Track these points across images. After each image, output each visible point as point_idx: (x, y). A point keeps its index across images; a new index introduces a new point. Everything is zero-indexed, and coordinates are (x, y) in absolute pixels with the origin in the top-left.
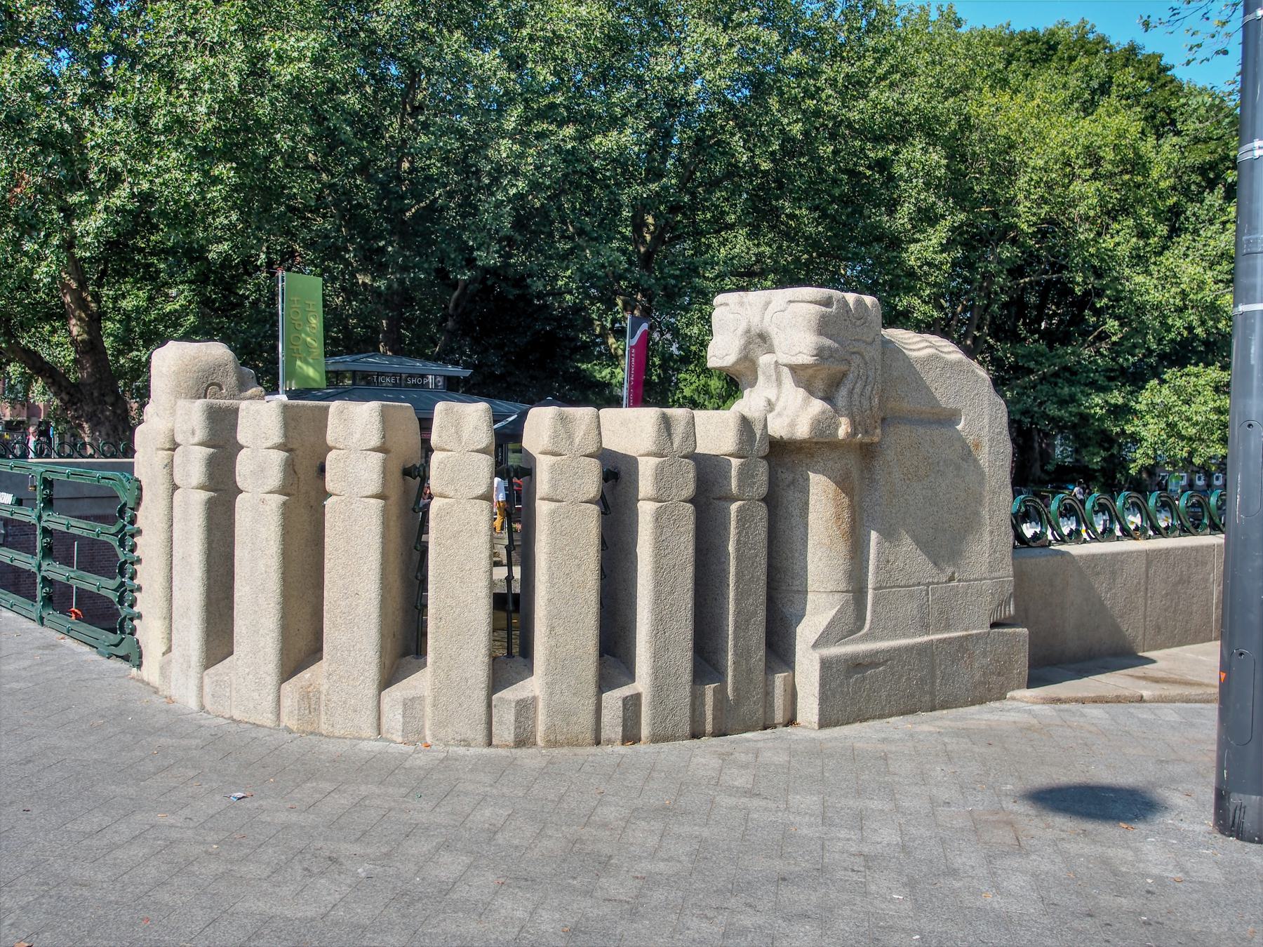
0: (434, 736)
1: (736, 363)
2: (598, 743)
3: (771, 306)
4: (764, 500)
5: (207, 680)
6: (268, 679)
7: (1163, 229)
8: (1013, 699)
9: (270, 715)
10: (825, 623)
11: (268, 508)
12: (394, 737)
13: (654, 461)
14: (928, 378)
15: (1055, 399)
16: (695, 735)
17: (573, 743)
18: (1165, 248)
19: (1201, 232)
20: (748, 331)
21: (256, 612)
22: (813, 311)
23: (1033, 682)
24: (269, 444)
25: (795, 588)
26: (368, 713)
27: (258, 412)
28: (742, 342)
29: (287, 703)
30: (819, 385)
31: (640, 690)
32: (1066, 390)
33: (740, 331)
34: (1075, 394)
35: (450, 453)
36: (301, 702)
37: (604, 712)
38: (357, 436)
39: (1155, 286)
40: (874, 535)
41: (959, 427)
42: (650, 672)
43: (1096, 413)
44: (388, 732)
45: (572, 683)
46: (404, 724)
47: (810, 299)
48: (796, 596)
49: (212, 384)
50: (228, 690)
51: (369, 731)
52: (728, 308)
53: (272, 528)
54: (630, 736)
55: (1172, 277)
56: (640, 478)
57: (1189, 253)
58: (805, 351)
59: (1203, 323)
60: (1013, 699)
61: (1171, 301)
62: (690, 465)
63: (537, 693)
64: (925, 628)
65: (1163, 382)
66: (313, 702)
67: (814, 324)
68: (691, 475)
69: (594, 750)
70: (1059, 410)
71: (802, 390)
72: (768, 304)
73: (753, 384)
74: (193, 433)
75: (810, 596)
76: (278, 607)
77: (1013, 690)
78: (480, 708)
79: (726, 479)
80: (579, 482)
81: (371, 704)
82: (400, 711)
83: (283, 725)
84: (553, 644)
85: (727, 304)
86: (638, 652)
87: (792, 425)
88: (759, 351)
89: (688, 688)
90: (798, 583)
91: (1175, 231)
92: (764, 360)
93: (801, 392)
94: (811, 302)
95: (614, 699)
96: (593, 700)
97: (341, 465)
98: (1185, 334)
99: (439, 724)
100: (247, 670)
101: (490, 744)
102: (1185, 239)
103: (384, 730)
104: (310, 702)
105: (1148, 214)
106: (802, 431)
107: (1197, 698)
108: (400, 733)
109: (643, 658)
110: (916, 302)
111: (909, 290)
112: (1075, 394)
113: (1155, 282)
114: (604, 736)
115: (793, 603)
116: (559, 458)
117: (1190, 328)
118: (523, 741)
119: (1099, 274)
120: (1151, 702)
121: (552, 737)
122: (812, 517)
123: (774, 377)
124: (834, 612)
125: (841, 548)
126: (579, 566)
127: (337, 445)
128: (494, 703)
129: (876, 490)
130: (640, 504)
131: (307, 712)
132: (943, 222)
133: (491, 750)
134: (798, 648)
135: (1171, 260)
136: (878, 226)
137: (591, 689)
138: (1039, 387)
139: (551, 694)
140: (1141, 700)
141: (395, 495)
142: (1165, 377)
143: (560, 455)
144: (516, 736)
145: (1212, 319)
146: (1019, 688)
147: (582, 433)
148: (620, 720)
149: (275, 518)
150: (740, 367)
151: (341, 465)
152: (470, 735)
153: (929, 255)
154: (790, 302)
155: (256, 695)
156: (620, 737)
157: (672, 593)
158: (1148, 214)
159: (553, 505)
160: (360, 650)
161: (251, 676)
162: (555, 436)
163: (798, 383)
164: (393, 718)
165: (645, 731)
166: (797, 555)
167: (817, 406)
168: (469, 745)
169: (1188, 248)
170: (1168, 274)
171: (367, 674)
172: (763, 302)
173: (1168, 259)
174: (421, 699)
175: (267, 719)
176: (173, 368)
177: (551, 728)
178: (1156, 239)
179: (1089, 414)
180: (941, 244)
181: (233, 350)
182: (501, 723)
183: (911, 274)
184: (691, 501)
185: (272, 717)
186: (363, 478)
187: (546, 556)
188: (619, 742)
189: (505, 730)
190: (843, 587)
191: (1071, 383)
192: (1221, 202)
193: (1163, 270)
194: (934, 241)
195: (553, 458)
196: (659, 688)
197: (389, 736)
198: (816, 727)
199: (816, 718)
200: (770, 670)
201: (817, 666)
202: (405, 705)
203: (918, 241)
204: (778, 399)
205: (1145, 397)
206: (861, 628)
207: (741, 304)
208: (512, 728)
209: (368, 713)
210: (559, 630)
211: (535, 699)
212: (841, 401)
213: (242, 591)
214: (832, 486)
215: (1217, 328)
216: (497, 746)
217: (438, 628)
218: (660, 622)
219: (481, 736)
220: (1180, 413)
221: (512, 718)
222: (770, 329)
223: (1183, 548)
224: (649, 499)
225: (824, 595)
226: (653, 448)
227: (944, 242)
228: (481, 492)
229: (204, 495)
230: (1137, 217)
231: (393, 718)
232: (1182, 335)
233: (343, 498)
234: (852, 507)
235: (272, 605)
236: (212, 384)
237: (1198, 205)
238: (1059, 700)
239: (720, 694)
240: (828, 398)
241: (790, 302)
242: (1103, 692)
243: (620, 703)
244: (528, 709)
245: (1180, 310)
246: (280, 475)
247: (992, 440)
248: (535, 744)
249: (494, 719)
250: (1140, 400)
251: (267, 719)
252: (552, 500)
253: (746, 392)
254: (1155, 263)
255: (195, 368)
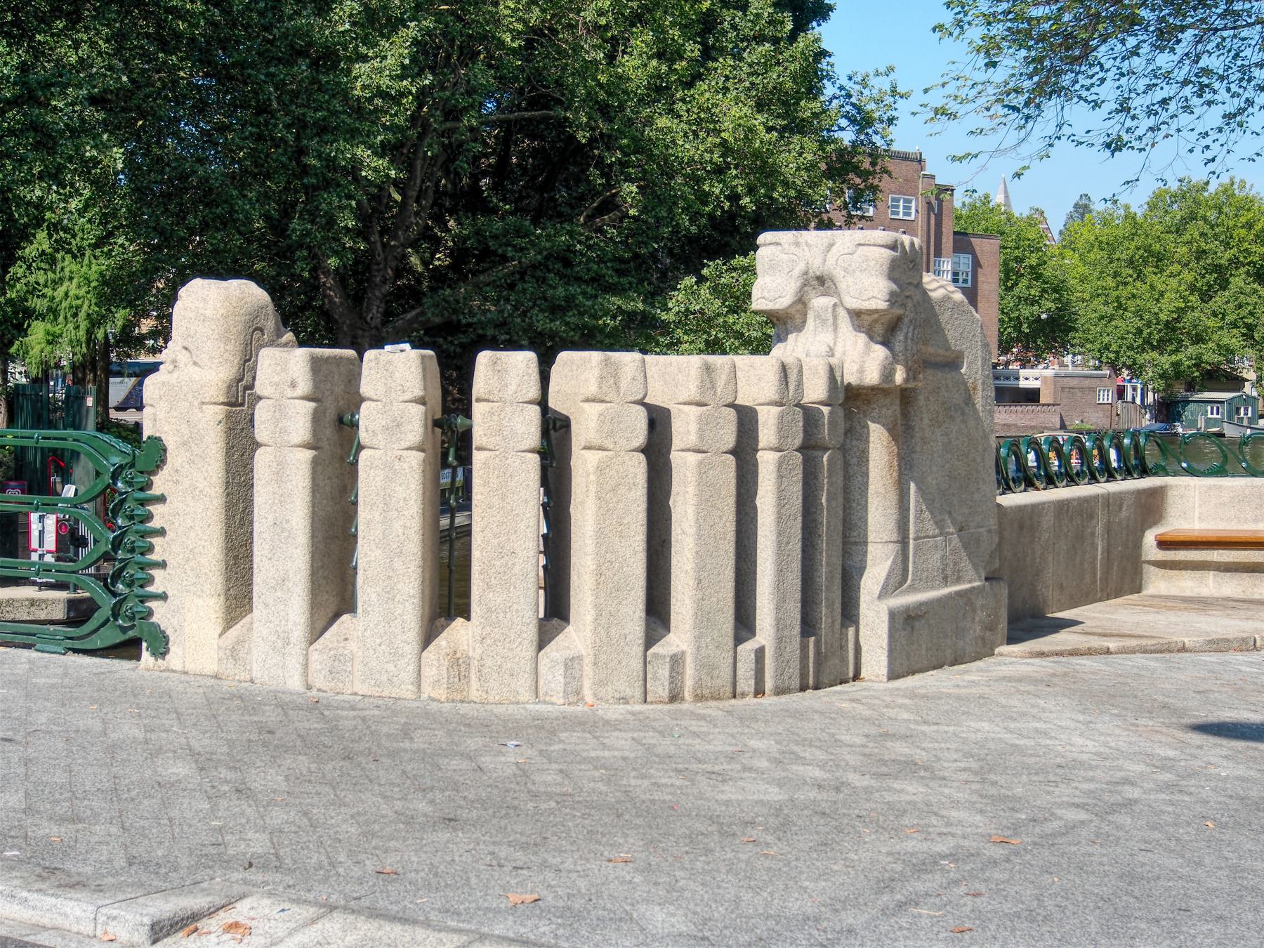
0: (595, 695)
1: (791, 306)
2: (735, 697)
3: (834, 248)
4: (731, 452)
5: (314, 656)
6: (408, 648)
7: (693, 50)
8: (1001, 654)
9: (410, 687)
10: (884, 574)
11: (406, 466)
12: (554, 699)
13: (775, 410)
14: (944, 318)
15: (545, 305)
16: (803, 688)
17: (716, 697)
18: (699, 77)
19: (745, 55)
20: (806, 273)
21: (389, 577)
22: (885, 256)
23: (1011, 640)
24: (408, 396)
25: (853, 540)
26: (526, 676)
27: (390, 362)
28: (799, 284)
29: (429, 673)
30: (879, 329)
31: (763, 642)
32: (561, 291)
33: (797, 271)
34: (574, 297)
35: (608, 405)
36: (451, 670)
37: (738, 665)
38: (513, 388)
39: (686, 135)
40: (912, 485)
41: (963, 371)
42: (774, 623)
43: (606, 325)
44: (546, 694)
45: (715, 636)
46: (566, 684)
47: (881, 243)
48: (854, 548)
49: (256, 329)
50: (349, 665)
51: (526, 695)
52: (779, 248)
53: (413, 487)
54: (759, 691)
55: (706, 122)
56: (760, 428)
57: (729, 84)
58: (879, 296)
59: (751, 190)
60: (1001, 654)
61: (707, 156)
62: (732, 414)
63: (684, 647)
64: (946, 581)
65: (701, 280)
66: (462, 669)
67: (885, 268)
68: (801, 424)
69: (733, 701)
70: (552, 321)
71: (863, 335)
72: (831, 245)
73: (800, 328)
74: (293, 385)
75: (870, 548)
76: (419, 571)
77: (999, 646)
78: (637, 665)
79: (816, 426)
80: (722, 432)
81: (529, 667)
82: (561, 672)
83: (424, 696)
84: (700, 596)
85: (778, 244)
86: (758, 604)
87: (861, 371)
88: (812, 293)
89: (798, 639)
90: (855, 534)
91: (708, 53)
92: (820, 303)
93: (862, 338)
94: (882, 246)
95: (747, 648)
96: (732, 652)
97: (495, 418)
98: (727, 205)
99: (600, 683)
100: (378, 641)
101: (645, 701)
102: (723, 64)
103: (541, 693)
104: (459, 666)
105: (673, 24)
106: (872, 376)
107: (1153, 648)
108: (561, 695)
109: (766, 610)
110: (362, 152)
111: (353, 135)
112: (574, 297)
113: (686, 127)
114: (739, 690)
115: (851, 554)
116: (705, 408)
117: (734, 198)
118: (674, 697)
119: (605, 110)
120: (1116, 653)
121: (699, 692)
122: (872, 464)
123: (831, 321)
124: (889, 562)
125: (893, 497)
126: (721, 517)
127: (491, 398)
128: (648, 659)
129: (912, 437)
130: (760, 454)
131: (456, 680)
132: (403, 32)
133: (645, 707)
134: (862, 599)
135: (707, 95)
136: (306, 33)
137: (731, 642)
138: (520, 286)
139: (698, 647)
140: (1108, 652)
141: (428, 446)
142: (705, 271)
143: (706, 405)
144: (671, 691)
145: (763, 185)
146: (1001, 644)
147: (723, 383)
148: (753, 673)
149: (416, 476)
150: (792, 311)
151: (495, 418)
152: (629, 692)
153: (385, 82)
154: (859, 245)
155: (391, 667)
156: (752, 690)
157: (788, 543)
158: (673, 24)
159: (700, 456)
160: (517, 611)
161: (383, 647)
162: (702, 386)
163: (858, 328)
164: (552, 679)
165: (769, 684)
166: (854, 505)
167: (880, 352)
168: (627, 703)
169: (727, 78)
170: (703, 115)
171: (525, 635)
172: (826, 244)
173: (703, 92)
174: (580, 658)
175: (407, 691)
176: (222, 311)
177: (699, 683)
178: (684, 63)
179: (596, 327)
180: (403, 66)
181: (267, 290)
182: (655, 679)
183: (358, 110)
184: (731, 452)
185: (414, 688)
186: (519, 432)
187: (694, 508)
188: (751, 695)
189: (659, 688)
190: (894, 538)
191: (567, 280)
192: (771, 10)
193: (695, 110)
194: (390, 61)
195: (699, 408)
196: (780, 640)
197: (547, 699)
198: (885, 679)
199: (884, 671)
200: (844, 626)
201: (886, 618)
202: (566, 665)
203: (365, 59)
204: (835, 344)
205: (677, 301)
206: (905, 581)
207: (797, 244)
208: (667, 683)
209: (526, 676)
210: (705, 583)
211: (683, 653)
212: (898, 347)
213: (368, 555)
214: (886, 434)
215: (771, 198)
216: (652, 703)
217: (599, 584)
218: (780, 572)
219: (638, 694)
220: (726, 327)
221: (667, 674)
222: (834, 272)
223: (1079, 499)
224: (771, 449)
225: (880, 546)
226: (776, 397)
227: (407, 62)
228: (638, 444)
229: (309, 454)
230: (659, 30)
231: (552, 679)
232: (722, 208)
233: (498, 453)
234: (901, 457)
235: (413, 568)
236: (256, 329)
237: (740, 14)
238: (1041, 654)
239: (817, 644)
240: (885, 343)
241: (859, 245)
242: (1046, 649)
243: (753, 656)
244: (679, 664)
245: (719, 171)
246: (421, 430)
247: (984, 383)
248: (683, 699)
249: (649, 676)
250: (670, 305)
251: (407, 691)
252: (699, 451)
253: (791, 337)
254: (683, 100)
255: (242, 312)
